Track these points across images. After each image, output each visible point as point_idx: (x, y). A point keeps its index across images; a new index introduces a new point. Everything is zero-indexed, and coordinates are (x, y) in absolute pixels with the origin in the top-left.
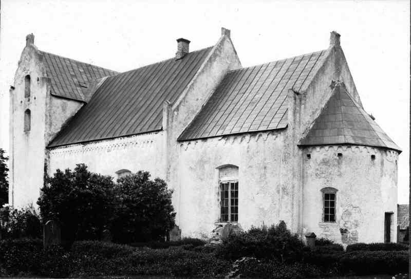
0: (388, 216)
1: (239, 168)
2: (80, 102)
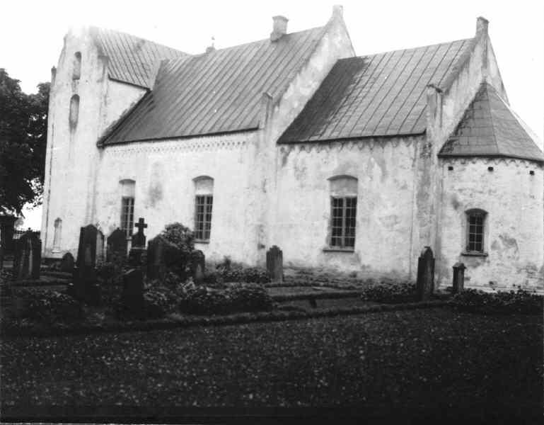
1: (215, 182)
2: (144, 88)
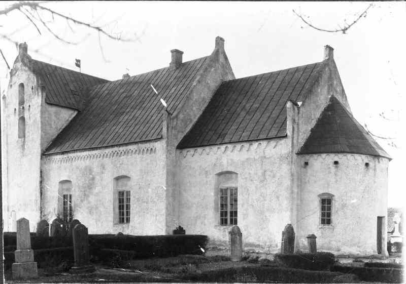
0: (380, 219)
